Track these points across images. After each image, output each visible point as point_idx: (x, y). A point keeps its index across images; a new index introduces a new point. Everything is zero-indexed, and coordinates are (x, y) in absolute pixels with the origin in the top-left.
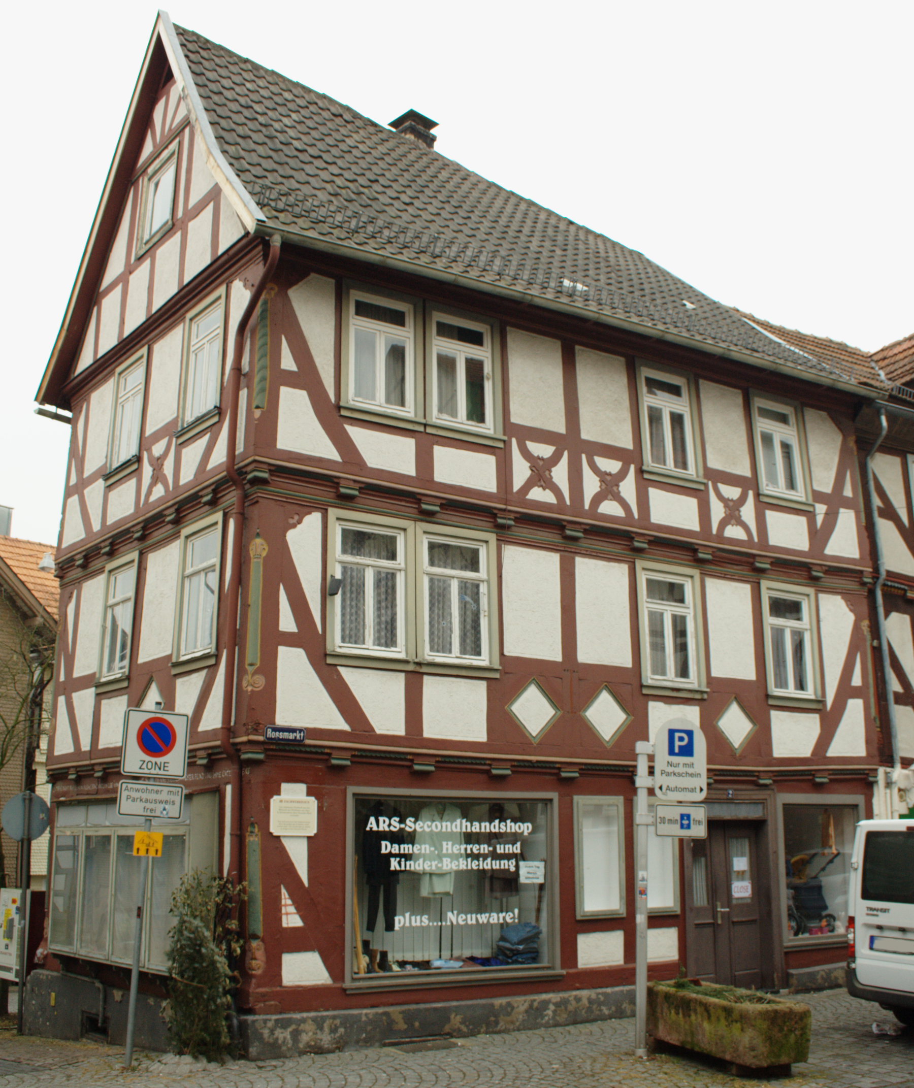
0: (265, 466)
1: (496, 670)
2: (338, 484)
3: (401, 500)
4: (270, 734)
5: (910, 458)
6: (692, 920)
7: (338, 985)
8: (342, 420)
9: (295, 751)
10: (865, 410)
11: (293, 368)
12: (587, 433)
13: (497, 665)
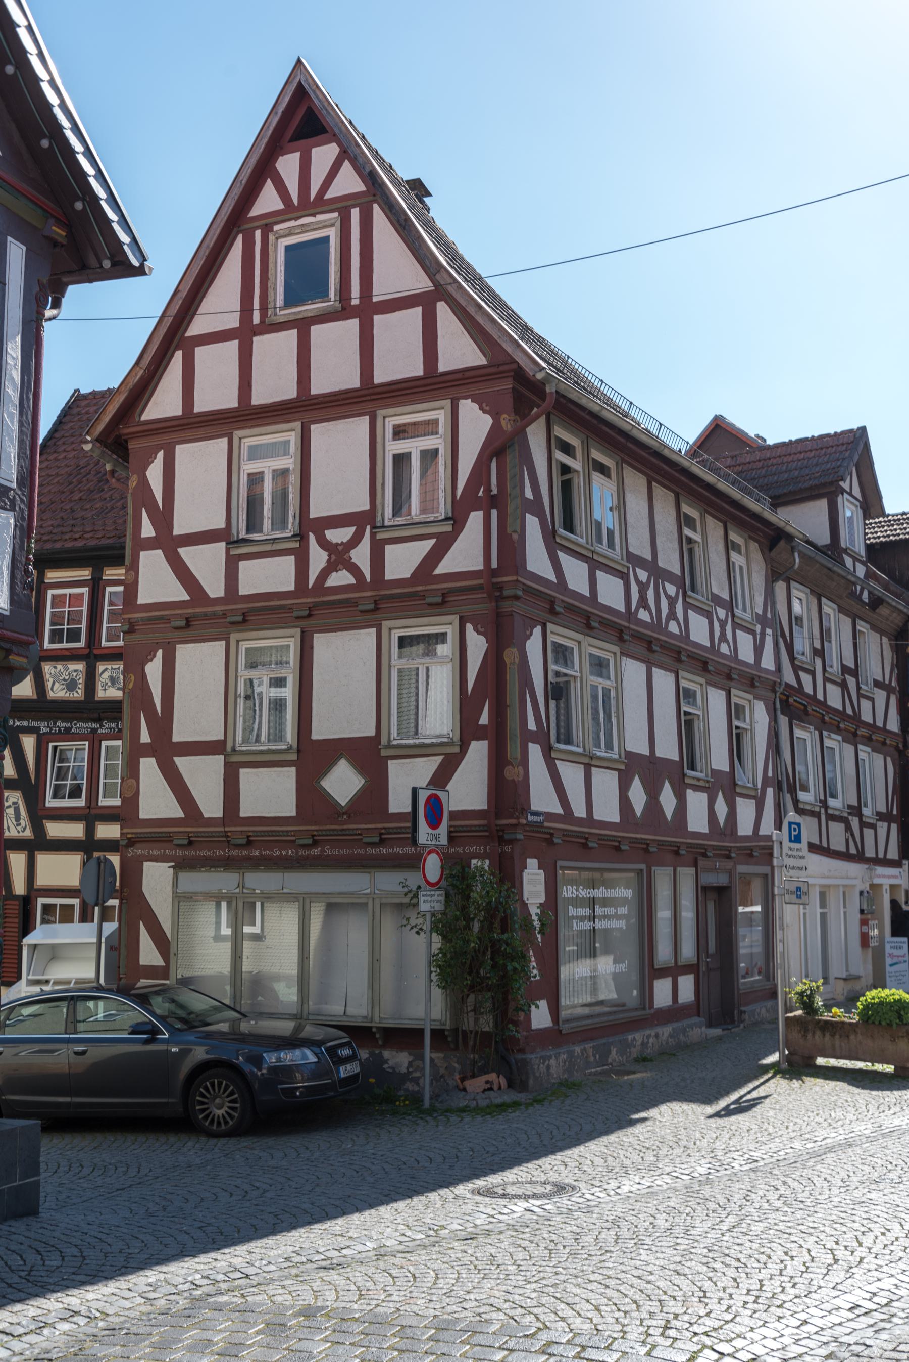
0: (521, 585)
4: (531, 818)
6: (703, 968)
7: (556, 1027)
11: (531, 497)
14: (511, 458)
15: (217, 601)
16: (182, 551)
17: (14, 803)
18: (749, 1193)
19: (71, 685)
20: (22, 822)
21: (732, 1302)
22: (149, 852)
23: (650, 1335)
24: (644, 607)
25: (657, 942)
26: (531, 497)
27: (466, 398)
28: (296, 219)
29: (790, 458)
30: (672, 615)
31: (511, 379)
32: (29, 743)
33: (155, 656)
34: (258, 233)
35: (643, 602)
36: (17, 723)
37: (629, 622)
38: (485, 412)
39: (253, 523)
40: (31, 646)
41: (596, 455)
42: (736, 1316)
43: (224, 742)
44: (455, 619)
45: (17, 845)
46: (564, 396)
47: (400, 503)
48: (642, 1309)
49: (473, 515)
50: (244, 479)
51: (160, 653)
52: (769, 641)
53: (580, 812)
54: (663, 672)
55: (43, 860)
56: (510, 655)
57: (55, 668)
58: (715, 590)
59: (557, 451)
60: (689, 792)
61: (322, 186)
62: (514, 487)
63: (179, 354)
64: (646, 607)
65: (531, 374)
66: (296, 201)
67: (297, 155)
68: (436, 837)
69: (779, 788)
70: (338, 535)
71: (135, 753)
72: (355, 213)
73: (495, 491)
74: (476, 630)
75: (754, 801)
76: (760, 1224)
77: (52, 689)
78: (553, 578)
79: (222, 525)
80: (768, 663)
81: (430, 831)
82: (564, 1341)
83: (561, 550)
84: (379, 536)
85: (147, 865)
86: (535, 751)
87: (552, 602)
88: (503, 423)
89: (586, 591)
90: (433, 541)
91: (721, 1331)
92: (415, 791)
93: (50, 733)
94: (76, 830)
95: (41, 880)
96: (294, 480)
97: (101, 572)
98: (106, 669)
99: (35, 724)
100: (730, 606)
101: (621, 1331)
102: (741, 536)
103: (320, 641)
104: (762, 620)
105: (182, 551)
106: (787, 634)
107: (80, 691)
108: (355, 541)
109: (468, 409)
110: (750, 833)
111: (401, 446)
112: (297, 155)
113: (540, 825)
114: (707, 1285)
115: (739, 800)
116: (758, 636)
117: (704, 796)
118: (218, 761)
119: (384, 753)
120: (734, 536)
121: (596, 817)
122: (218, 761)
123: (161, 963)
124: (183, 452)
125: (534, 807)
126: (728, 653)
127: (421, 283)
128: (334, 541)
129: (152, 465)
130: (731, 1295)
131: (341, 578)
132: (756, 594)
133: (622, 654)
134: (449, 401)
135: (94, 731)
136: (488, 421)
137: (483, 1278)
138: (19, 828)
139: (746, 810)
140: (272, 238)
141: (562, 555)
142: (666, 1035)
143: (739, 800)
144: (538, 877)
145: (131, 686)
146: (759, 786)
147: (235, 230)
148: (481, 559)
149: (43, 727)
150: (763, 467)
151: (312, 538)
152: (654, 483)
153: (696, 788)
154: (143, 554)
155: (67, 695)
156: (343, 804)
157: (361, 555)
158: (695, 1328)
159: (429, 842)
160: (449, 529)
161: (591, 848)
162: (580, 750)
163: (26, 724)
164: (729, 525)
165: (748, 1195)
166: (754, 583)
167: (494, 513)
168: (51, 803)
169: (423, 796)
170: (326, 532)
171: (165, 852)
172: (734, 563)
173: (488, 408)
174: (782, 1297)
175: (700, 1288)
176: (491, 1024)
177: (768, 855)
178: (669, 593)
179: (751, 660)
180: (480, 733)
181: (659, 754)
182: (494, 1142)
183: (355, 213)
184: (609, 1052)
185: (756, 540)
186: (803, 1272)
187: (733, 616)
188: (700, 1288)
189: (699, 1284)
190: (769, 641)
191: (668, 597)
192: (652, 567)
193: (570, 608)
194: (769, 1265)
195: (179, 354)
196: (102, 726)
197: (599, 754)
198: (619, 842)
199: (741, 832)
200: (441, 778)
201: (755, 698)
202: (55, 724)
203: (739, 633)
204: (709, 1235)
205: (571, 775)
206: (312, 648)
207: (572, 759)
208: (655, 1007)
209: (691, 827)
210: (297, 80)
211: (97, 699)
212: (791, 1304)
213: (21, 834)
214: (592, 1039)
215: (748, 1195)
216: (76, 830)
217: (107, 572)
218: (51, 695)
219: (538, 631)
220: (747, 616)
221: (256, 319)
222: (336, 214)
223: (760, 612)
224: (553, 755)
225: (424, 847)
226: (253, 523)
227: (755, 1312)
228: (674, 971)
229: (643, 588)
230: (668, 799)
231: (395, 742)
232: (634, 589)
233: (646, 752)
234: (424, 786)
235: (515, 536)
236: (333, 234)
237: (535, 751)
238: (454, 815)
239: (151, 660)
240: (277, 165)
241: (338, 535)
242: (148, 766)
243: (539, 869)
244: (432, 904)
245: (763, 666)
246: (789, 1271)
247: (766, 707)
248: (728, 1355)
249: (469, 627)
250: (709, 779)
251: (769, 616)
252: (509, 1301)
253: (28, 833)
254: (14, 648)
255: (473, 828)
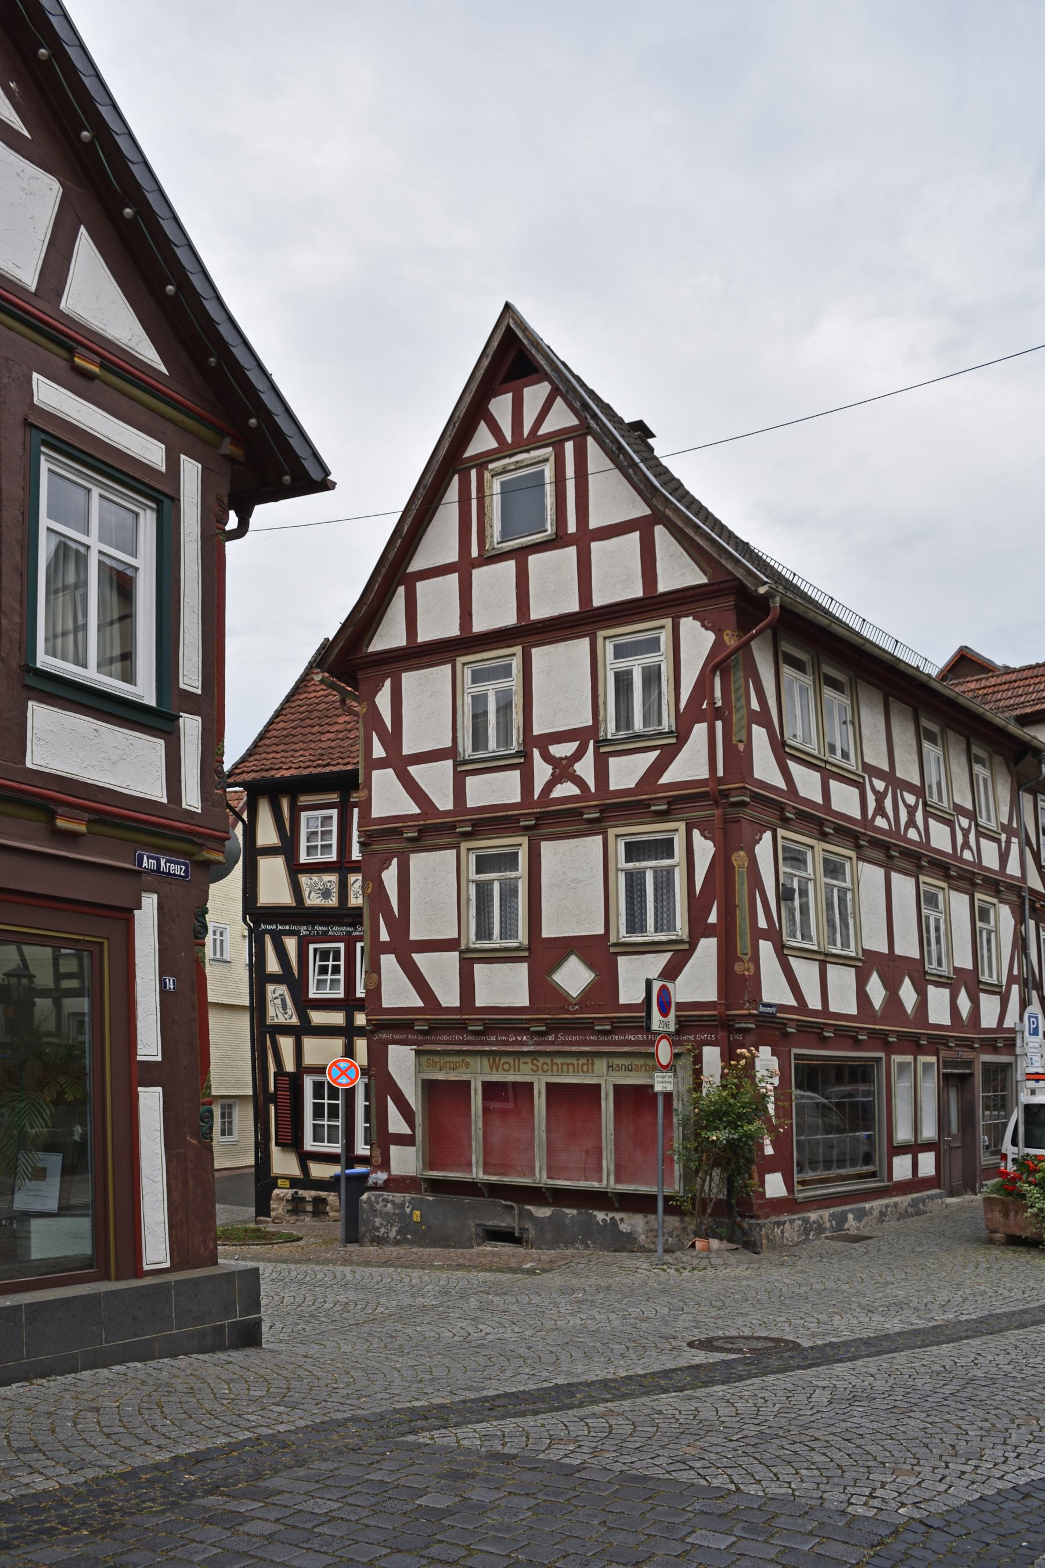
0: (748, 792)
1: (860, 960)
2: (823, 823)
3: (811, 823)
4: (762, 1009)
5: (1040, 797)
6: (943, 1147)
7: (791, 1197)
8: (785, 755)
9: (769, 1022)
10: (1029, 758)
11: (758, 709)
12: (453, 557)
13: (860, 956)
14: (738, 677)
15: (447, 813)
16: (412, 769)
17: (281, 995)
18: (978, 1357)
19: (326, 894)
20: (288, 1010)
21: (946, 1472)
22: (392, 1037)
23: (852, 1504)
24: (881, 815)
25: (896, 1123)
26: (758, 709)
27: (687, 616)
28: (511, 456)
29: (1037, 680)
30: (911, 823)
31: (734, 596)
32: (291, 944)
33: (390, 864)
34: (473, 473)
35: (880, 810)
36: (280, 927)
37: (865, 829)
38: (707, 629)
39: (479, 739)
40: (226, 843)
41: (827, 670)
42: (950, 1487)
43: (459, 939)
44: (682, 826)
45: (285, 1030)
46: (791, 612)
47: (624, 717)
48: (846, 1475)
49: (697, 726)
50: (468, 700)
51: (395, 861)
52: (1015, 848)
53: (814, 1002)
54: (902, 876)
55: (309, 1043)
56: (739, 858)
57: (311, 879)
58: (958, 801)
59: (785, 665)
60: (931, 989)
61: (535, 423)
62: (738, 700)
63: (401, 590)
64: (884, 815)
65: (753, 589)
66: (509, 440)
67: (510, 395)
68: (667, 1025)
69: (1025, 984)
70: (562, 750)
71: (377, 949)
72: (569, 446)
73: (719, 704)
74: (703, 835)
75: (998, 997)
76: (986, 1388)
77: (309, 897)
78: (781, 784)
79: (449, 744)
80: (1013, 868)
81: (662, 1019)
82: (756, 1507)
83: (790, 760)
84: (602, 750)
85: (392, 1048)
86: (766, 948)
87: (781, 807)
88: (726, 638)
89: (819, 799)
90: (658, 752)
91: (931, 1503)
92: (649, 983)
93: (309, 935)
94: (337, 1018)
95: (308, 1060)
96: (518, 700)
97: (349, 796)
98: (357, 880)
99: (296, 928)
100: (972, 815)
101: (821, 1498)
102: (985, 750)
103: (547, 848)
104: (1007, 829)
105: (412, 769)
106: (1035, 846)
107: (334, 899)
108: (578, 755)
109: (689, 625)
110: (994, 1025)
111: (623, 664)
112: (510, 395)
113: (772, 1015)
114: (921, 1452)
115: (983, 996)
116: (1003, 845)
117: (946, 992)
118: (453, 958)
119: (612, 950)
120: (976, 750)
121: (831, 1009)
122: (453, 958)
123: (409, 1132)
124: (408, 679)
125: (766, 999)
126: (972, 860)
127: (641, 510)
128: (558, 755)
129: (380, 692)
130: (947, 1463)
131: (566, 790)
132: (1001, 805)
133: (859, 858)
134: (670, 620)
135: (349, 933)
136: (710, 637)
137: (683, 1433)
138: (286, 1016)
139: (989, 1006)
140: (487, 475)
141: (792, 765)
142: (905, 1204)
143: (983, 996)
144: (772, 1063)
145: (369, 891)
146: (1004, 983)
147: (451, 471)
148: (707, 768)
149: (304, 930)
150: (1008, 690)
151: (536, 752)
152: (891, 698)
153: (938, 984)
154: (375, 773)
155: (323, 902)
156: (575, 996)
157: (585, 768)
158: (903, 1498)
159: (661, 1029)
160: (674, 741)
161: (828, 1037)
162: (815, 948)
163: (287, 927)
164: (972, 739)
165: (976, 1359)
166: (999, 795)
167: (719, 724)
168: (313, 993)
169: (656, 986)
170: (550, 747)
171: (407, 1037)
172: (977, 775)
173: (710, 625)
174: (1004, 1468)
175: (914, 1455)
176: (725, 1192)
177: (1010, 1045)
178: (908, 802)
179: (995, 865)
180: (709, 931)
181: (898, 951)
182: (722, 1298)
183: (569, 446)
184: (846, 1219)
185: (1000, 754)
186: (1029, 1442)
187: (977, 825)
188: (914, 1455)
189: (914, 1450)
190: (1015, 848)
191: (907, 806)
192: (889, 777)
193: (801, 815)
194: (993, 1433)
195: (401, 590)
196: (356, 929)
197: (834, 951)
198: (857, 1032)
199: (984, 1024)
200: (671, 972)
201: (1000, 902)
202: (313, 928)
203: (982, 841)
204: (930, 1399)
205: (806, 972)
206: (540, 855)
207: (806, 954)
208: (894, 1180)
209: (932, 1020)
210: (506, 322)
211: (349, 906)
212: (1012, 1475)
213: (288, 1021)
214: (828, 1207)
215: (976, 1359)
216: (337, 1018)
217: (354, 795)
218: (308, 902)
219: (768, 836)
220: (993, 825)
221: (475, 553)
222: (550, 449)
223: (1006, 822)
224: (786, 952)
225: (657, 1033)
226: (479, 739)
227: (973, 1483)
228: (914, 1149)
229: (880, 797)
230: (908, 994)
231: (623, 940)
232: (871, 799)
233: (885, 950)
234: (656, 977)
235: (741, 746)
236: (549, 471)
237: (766, 948)
238: (680, 1006)
239: (387, 868)
240: (490, 407)
241: (560, 750)
242: (389, 962)
243: (773, 1055)
244: (664, 1085)
245: (1008, 872)
246: (1013, 1440)
247: (1011, 910)
248: (938, 1528)
249: (696, 833)
250: (951, 975)
251: (1015, 825)
252: (704, 1459)
253: (295, 1020)
254: (209, 844)
255: (705, 1018)
